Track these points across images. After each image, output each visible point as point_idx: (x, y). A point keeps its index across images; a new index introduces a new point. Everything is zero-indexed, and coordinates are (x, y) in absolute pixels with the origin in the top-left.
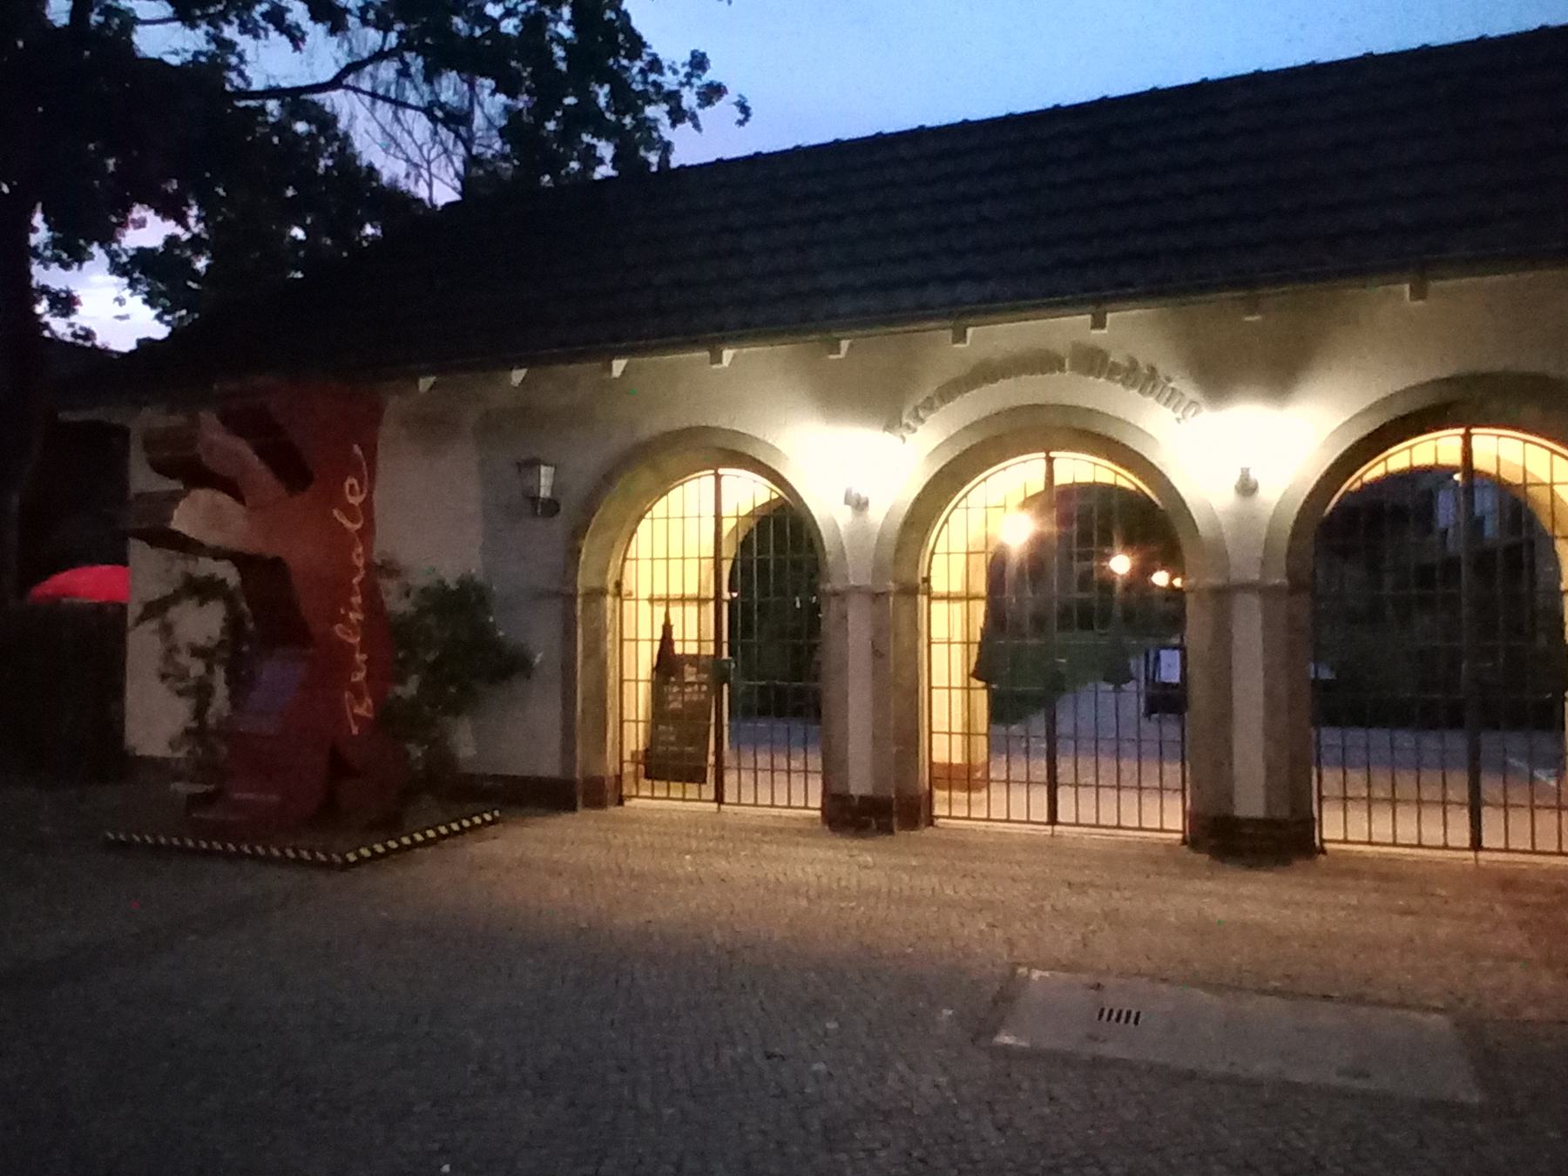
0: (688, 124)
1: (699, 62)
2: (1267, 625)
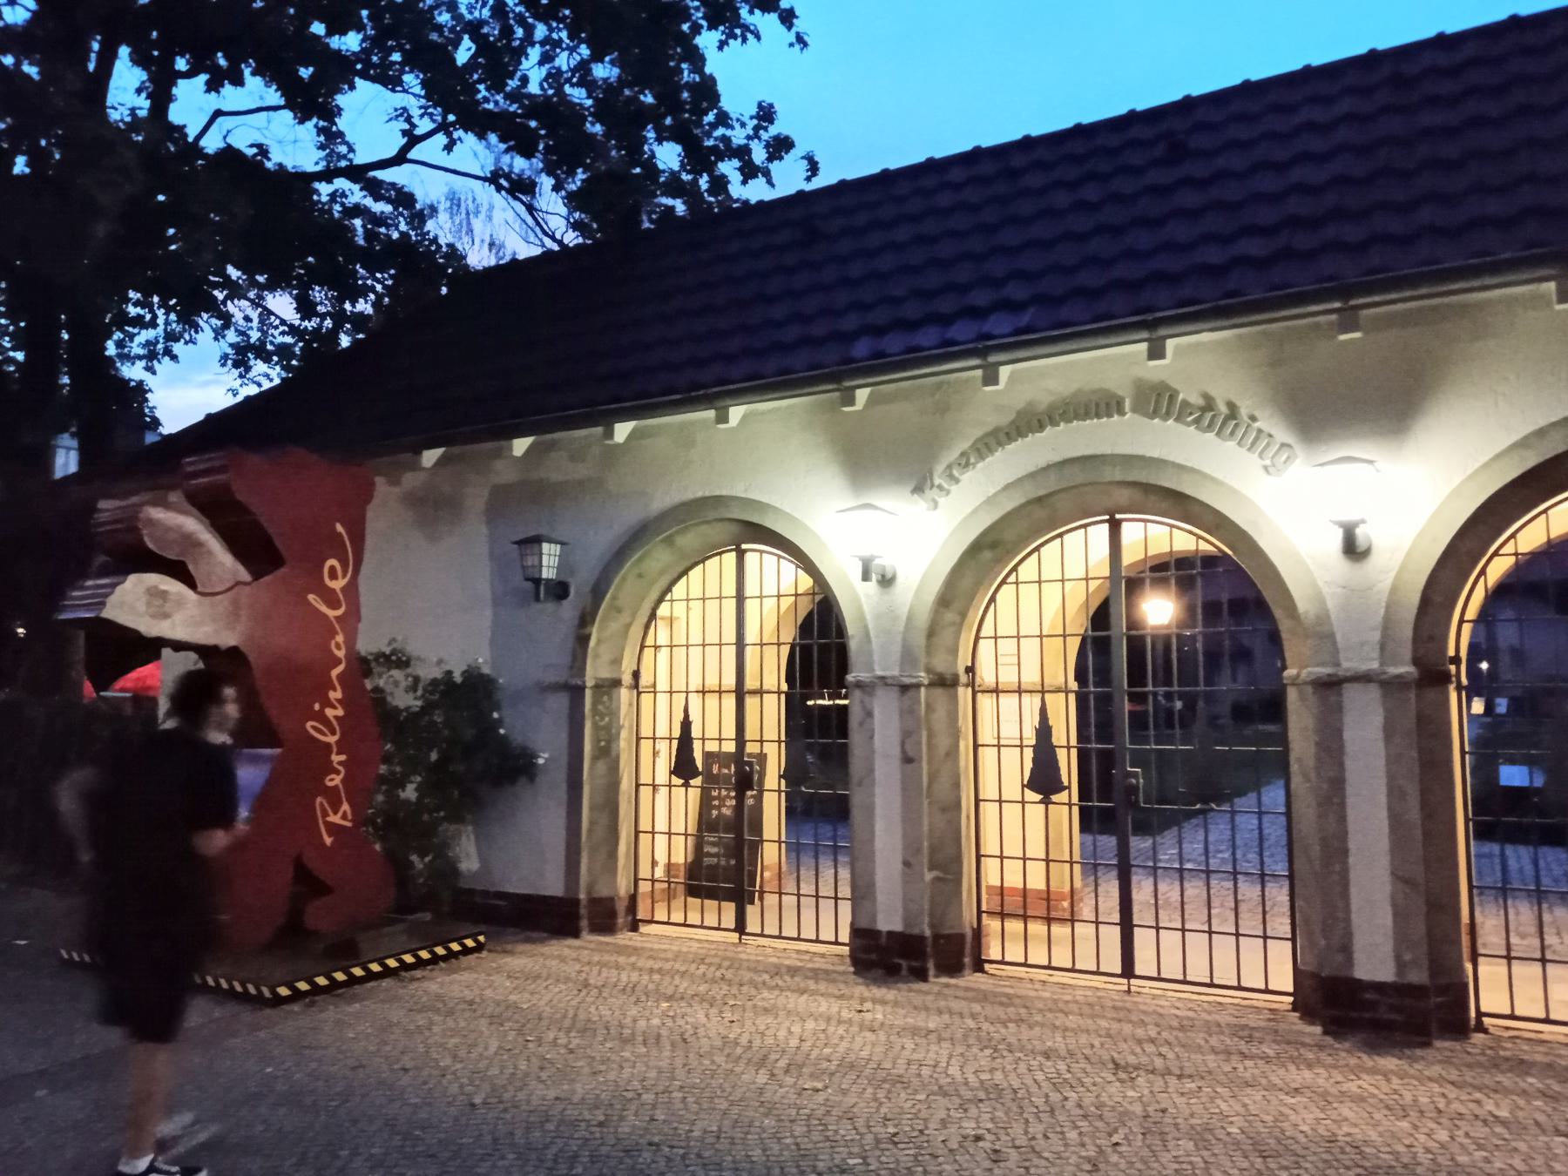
0: (761, 180)
1: (766, 114)
2: (1389, 731)
